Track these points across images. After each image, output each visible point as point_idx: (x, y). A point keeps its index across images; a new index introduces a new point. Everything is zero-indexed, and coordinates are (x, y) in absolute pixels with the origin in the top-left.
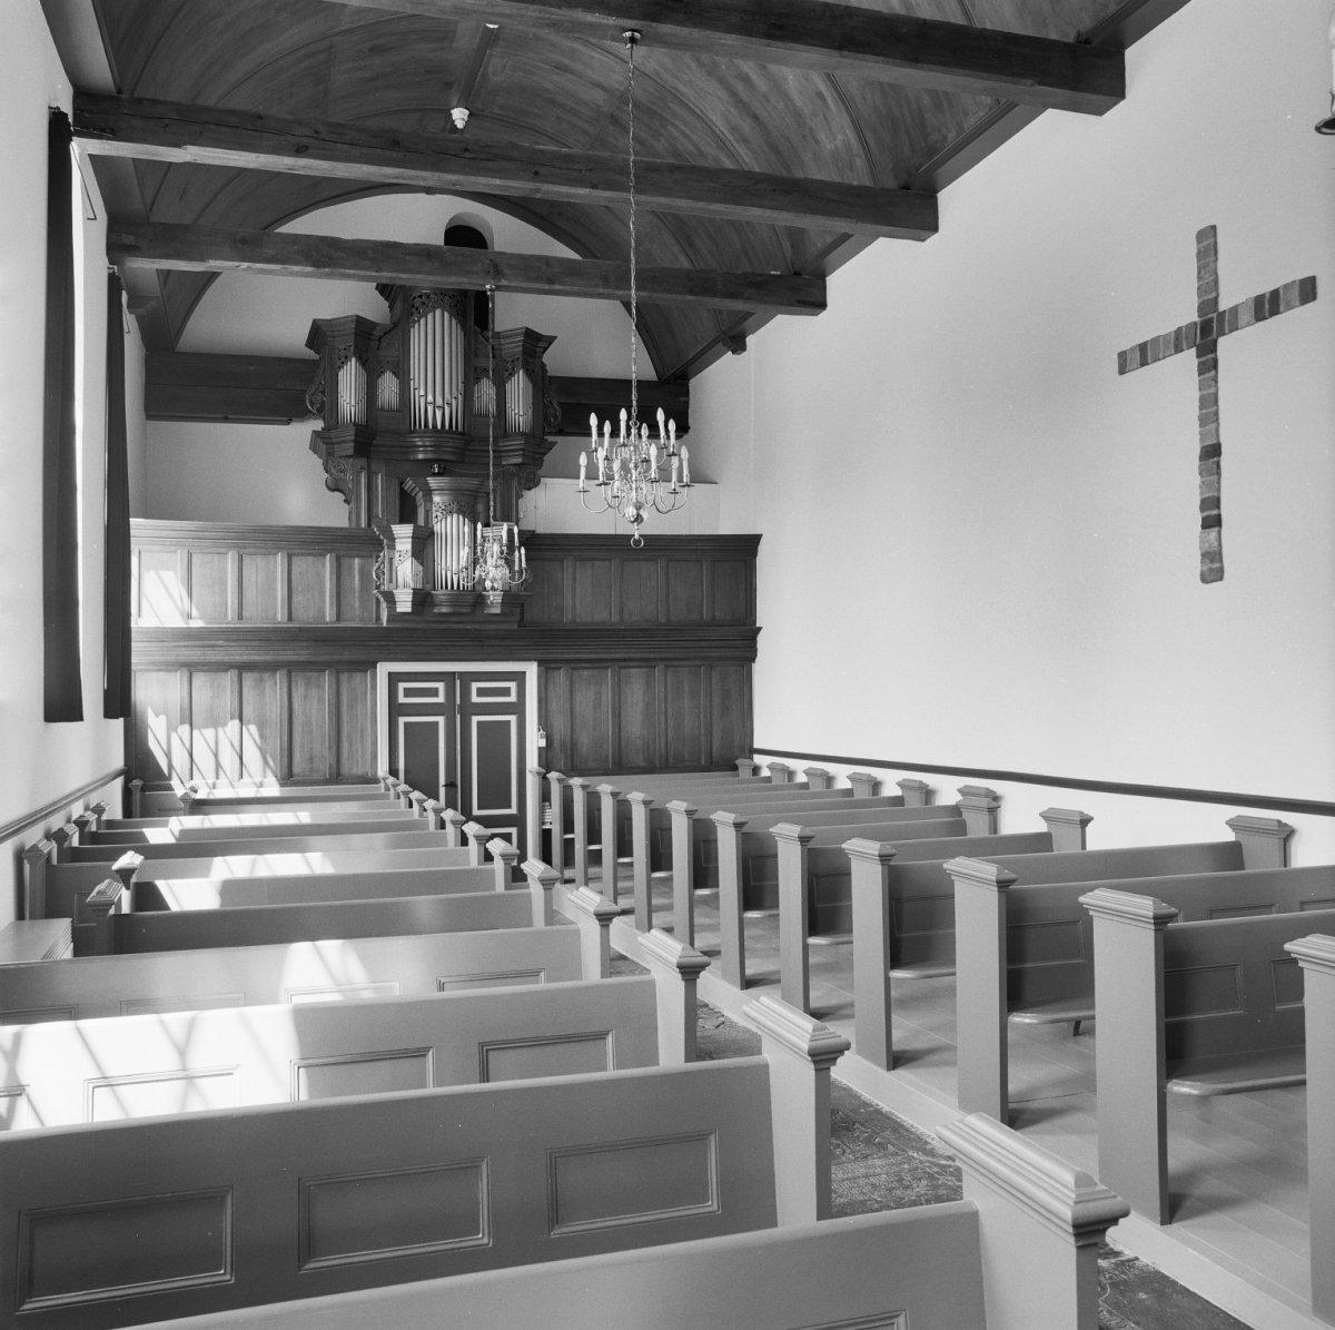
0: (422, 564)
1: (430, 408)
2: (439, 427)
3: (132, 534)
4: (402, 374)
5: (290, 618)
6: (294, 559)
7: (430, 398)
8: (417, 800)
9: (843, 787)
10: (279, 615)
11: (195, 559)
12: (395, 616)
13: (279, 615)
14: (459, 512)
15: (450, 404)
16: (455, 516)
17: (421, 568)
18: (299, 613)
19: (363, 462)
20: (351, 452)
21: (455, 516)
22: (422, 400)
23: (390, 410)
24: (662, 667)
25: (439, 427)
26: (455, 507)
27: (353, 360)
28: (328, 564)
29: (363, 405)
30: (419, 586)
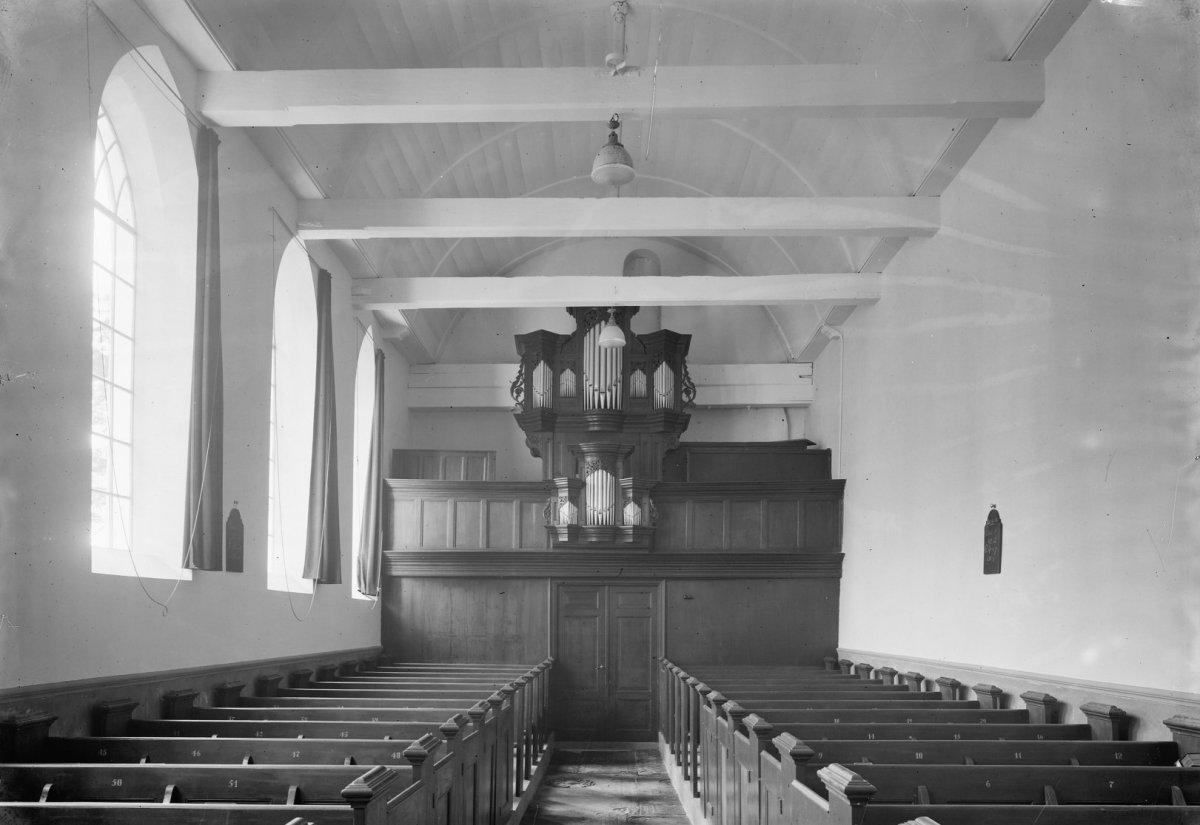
0: (577, 507)
1: (596, 394)
2: (603, 407)
3: (94, 486)
4: (578, 371)
5: (488, 546)
6: (491, 504)
7: (596, 386)
8: (701, 692)
9: (1018, 708)
10: (480, 543)
11: (426, 504)
12: (558, 545)
13: (480, 543)
14: (604, 468)
15: (611, 391)
16: (600, 471)
17: (576, 510)
18: (493, 544)
19: (549, 434)
20: (540, 427)
21: (600, 471)
22: (591, 388)
23: (641, 398)
24: (664, 582)
25: (603, 407)
26: (600, 464)
27: (542, 362)
28: (514, 507)
29: (549, 394)
30: (575, 522)
